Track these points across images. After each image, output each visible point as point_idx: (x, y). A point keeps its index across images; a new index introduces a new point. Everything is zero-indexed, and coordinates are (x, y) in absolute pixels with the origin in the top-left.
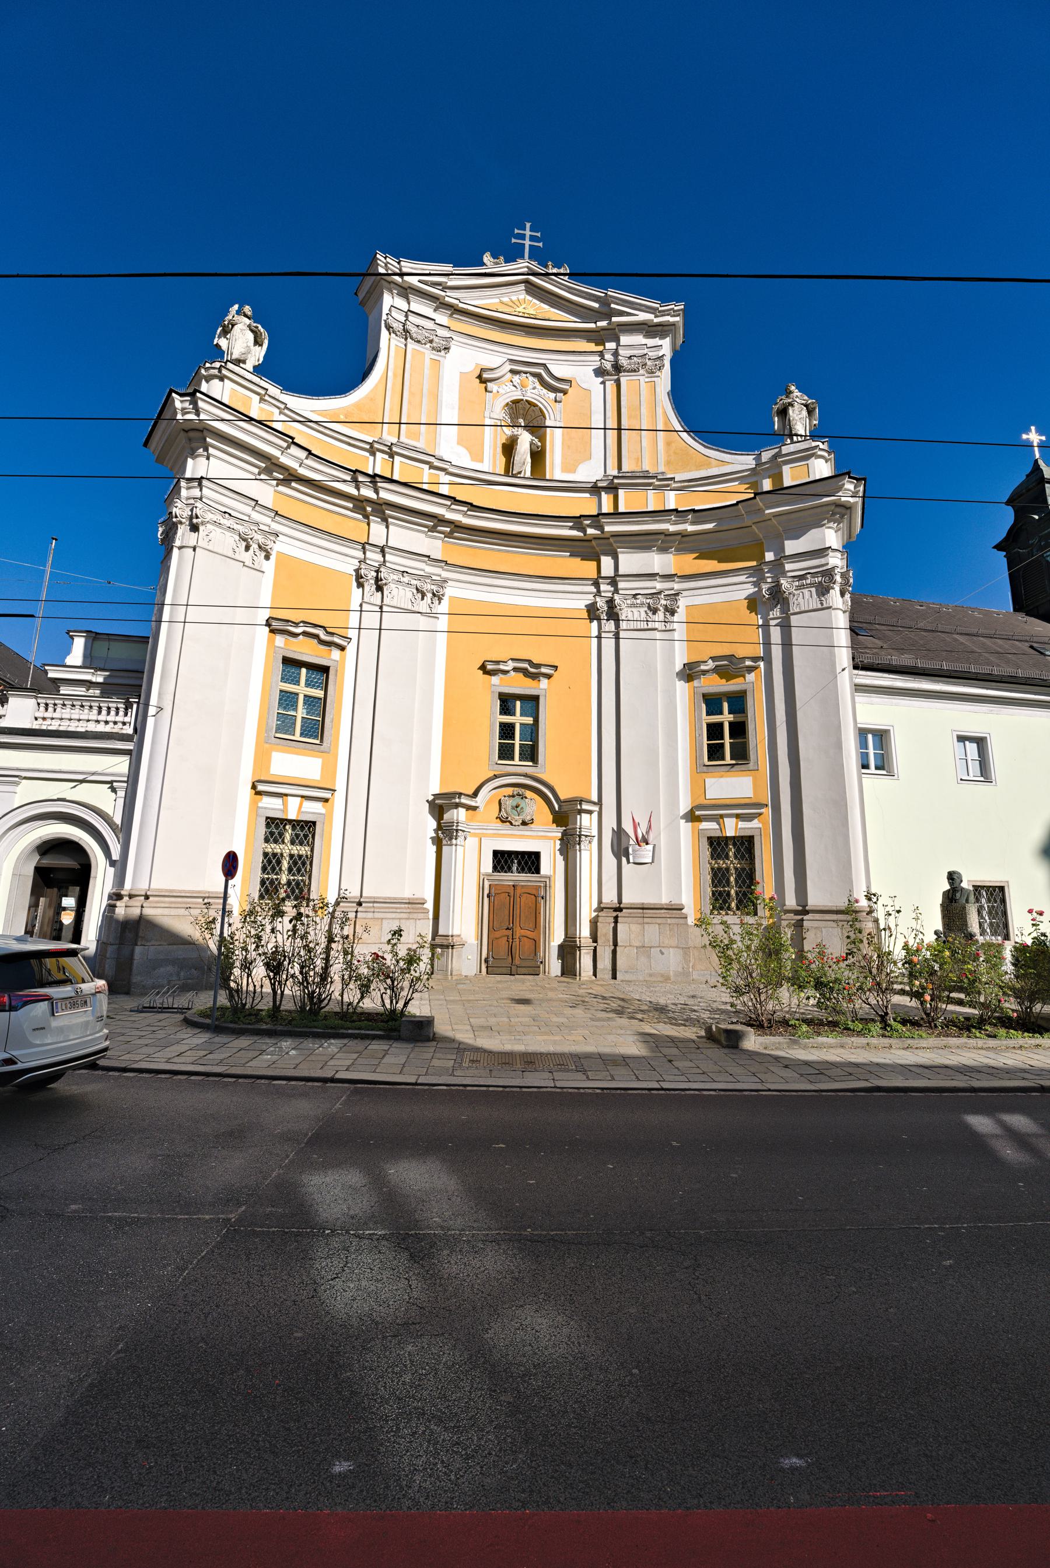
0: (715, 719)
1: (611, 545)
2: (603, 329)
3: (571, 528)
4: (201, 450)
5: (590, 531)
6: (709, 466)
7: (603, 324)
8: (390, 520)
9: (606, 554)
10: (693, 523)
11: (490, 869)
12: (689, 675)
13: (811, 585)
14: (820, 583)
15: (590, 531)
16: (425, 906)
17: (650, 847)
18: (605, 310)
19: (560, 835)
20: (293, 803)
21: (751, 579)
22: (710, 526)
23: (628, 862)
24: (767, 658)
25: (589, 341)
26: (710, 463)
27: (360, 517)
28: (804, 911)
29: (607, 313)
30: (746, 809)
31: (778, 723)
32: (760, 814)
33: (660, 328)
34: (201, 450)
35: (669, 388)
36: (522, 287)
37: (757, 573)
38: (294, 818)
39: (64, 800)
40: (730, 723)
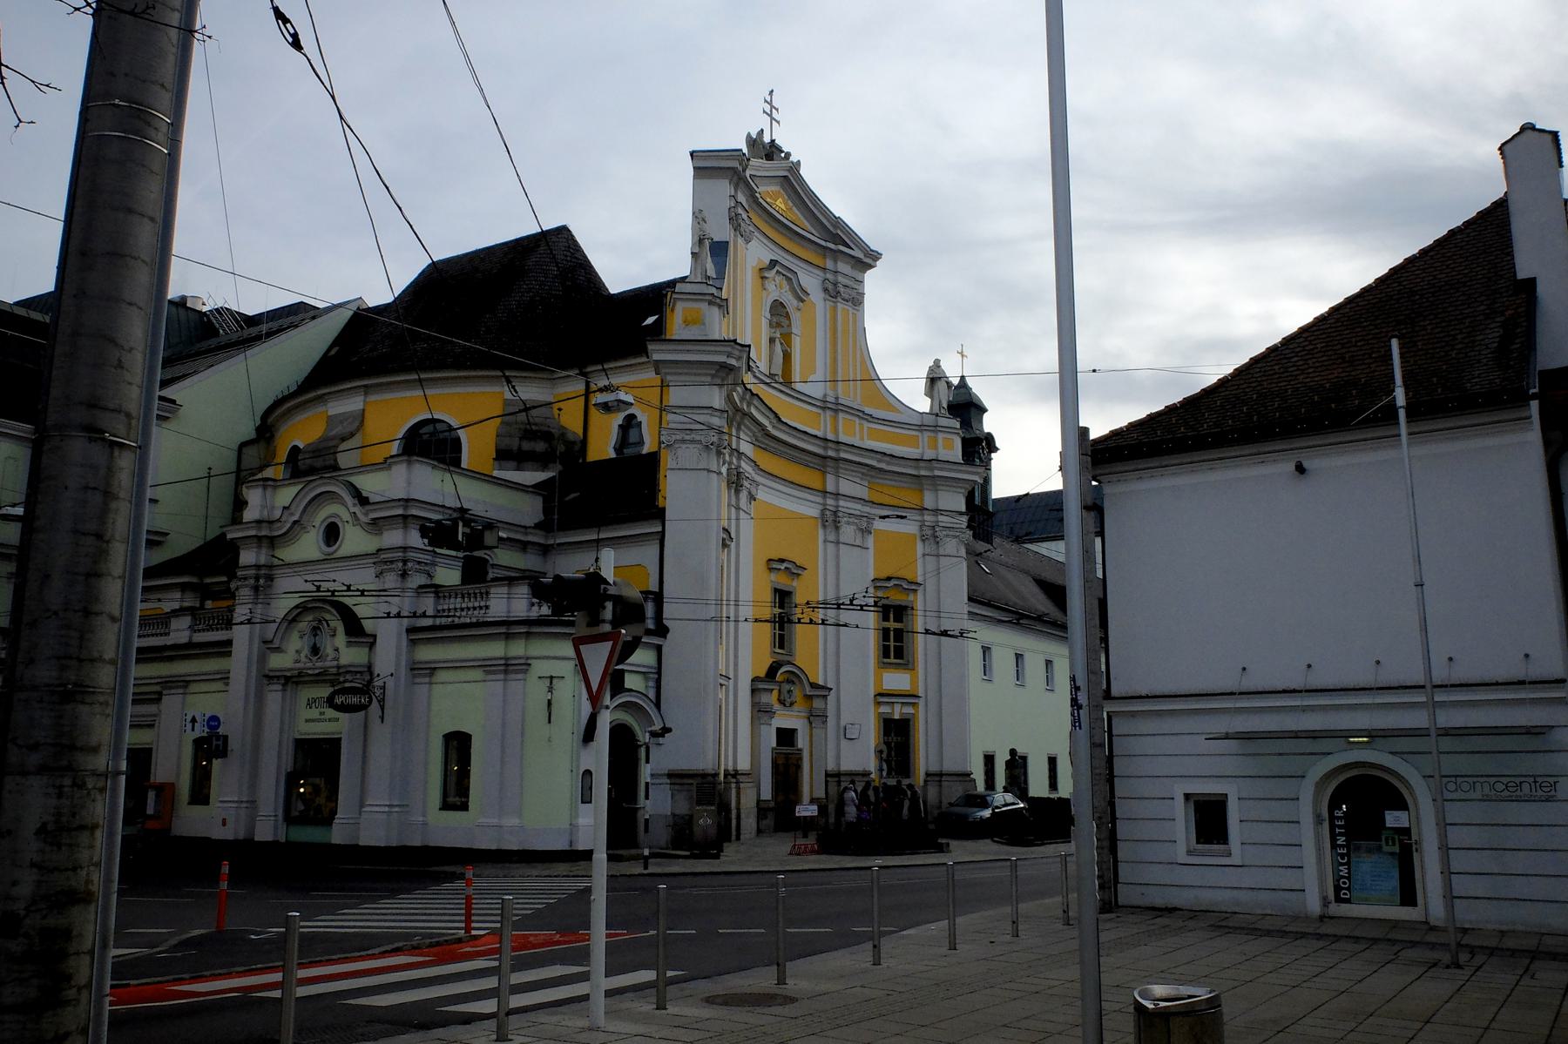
0: (886, 624)
20: (897, 708)
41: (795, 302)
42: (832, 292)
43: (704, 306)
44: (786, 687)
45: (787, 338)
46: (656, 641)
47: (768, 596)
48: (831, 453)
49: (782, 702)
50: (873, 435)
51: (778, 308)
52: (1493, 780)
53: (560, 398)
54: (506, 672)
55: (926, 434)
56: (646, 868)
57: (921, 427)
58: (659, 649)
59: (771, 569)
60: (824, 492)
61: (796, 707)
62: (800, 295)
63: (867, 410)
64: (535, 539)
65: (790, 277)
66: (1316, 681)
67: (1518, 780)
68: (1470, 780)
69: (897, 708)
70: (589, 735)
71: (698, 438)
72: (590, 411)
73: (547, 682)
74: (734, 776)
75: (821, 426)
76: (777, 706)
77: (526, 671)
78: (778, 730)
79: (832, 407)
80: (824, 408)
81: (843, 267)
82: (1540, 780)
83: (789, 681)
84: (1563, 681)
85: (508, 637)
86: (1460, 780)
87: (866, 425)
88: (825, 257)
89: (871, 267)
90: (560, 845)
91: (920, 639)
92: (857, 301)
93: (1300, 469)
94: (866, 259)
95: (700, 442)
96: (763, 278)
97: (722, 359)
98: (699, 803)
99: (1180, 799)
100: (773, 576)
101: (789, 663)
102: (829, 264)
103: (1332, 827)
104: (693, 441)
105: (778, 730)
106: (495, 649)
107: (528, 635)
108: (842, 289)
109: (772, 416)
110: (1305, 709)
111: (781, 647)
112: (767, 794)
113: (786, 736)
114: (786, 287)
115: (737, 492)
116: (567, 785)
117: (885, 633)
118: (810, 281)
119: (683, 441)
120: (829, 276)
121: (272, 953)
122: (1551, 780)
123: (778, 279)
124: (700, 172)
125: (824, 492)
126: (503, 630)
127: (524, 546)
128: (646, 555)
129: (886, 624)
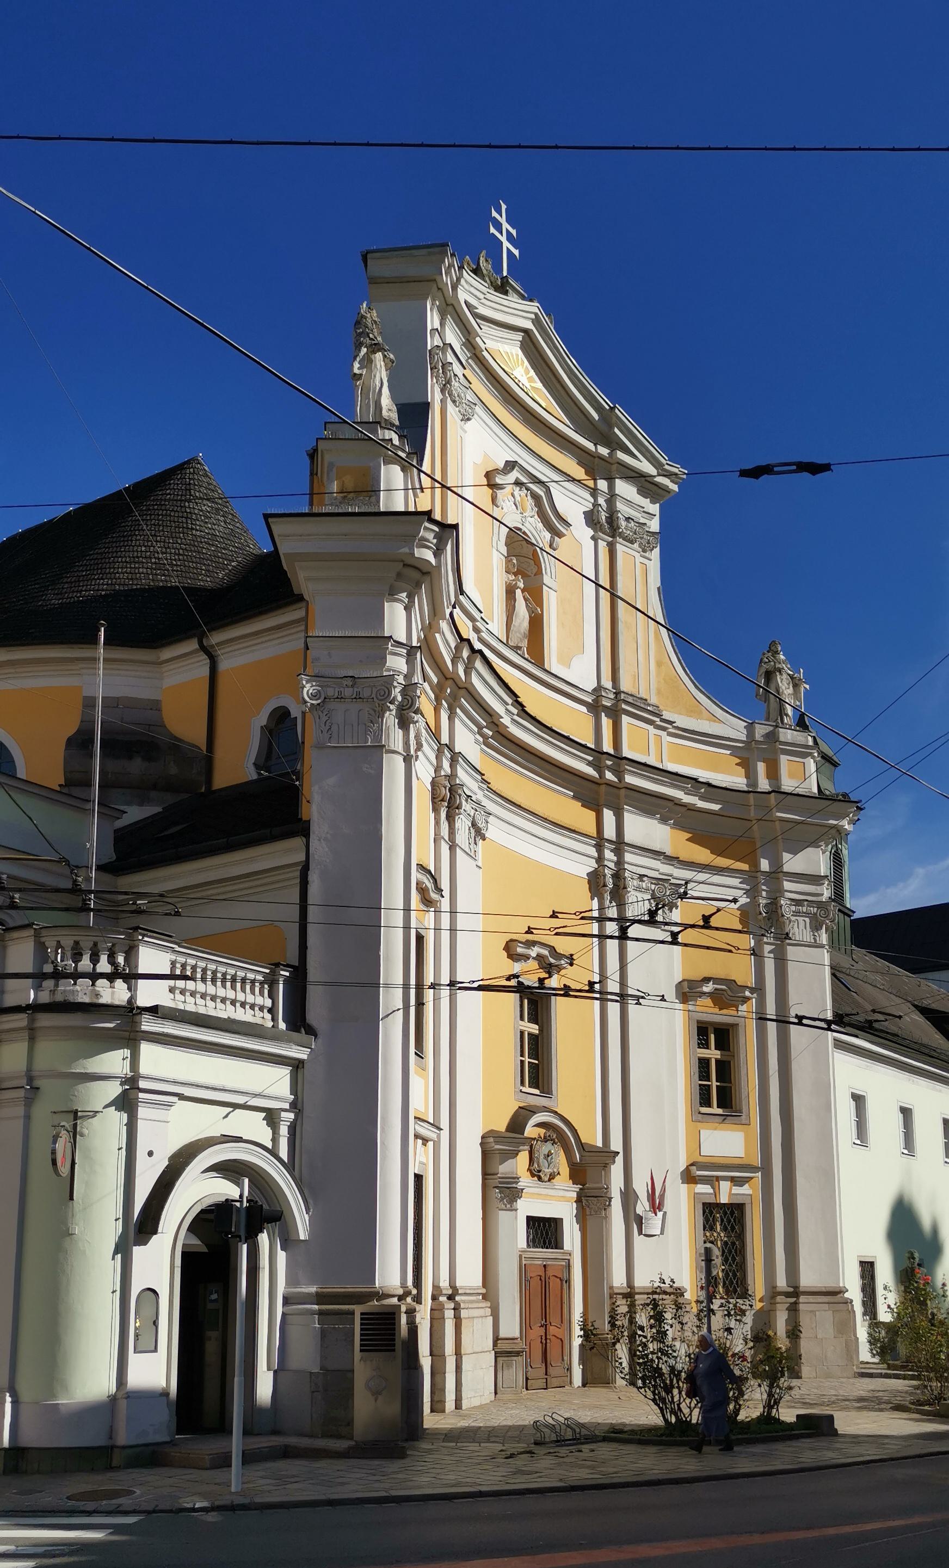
0: (704, 1053)
1: (618, 797)
2: (601, 458)
3: (590, 764)
4: (404, 595)
5: (609, 776)
6: (699, 715)
7: (604, 451)
8: (458, 711)
9: (609, 807)
10: (702, 798)
11: (525, 1245)
12: (684, 994)
13: (807, 914)
14: (815, 914)
15: (609, 776)
16: (846, 1295)
17: (662, 1213)
18: (603, 427)
19: (575, 1195)
20: (725, 1186)
21: (744, 886)
22: (716, 807)
23: (640, 1233)
24: (759, 989)
25: (580, 463)
26: (701, 712)
27: (433, 696)
28: (795, 1292)
29: (601, 433)
30: (736, 1171)
31: (771, 1072)
32: (752, 1178)
33: (656, 488)
34: (404, 595)
35: (659, 584)
36: (519, 336)
37: (752, 878)
38: (726, 1201)
39: (238, 1139)
40: (717, 1061)
45: (535, 595)
49: (535, 1174)
53: (171, 682)
62: (554, 523)
69: (725, 1186)
76: (525, 1181)
78: (531, 1221)
91: (825, 942)
98: (179, 1432)
101: (546, 1109)
105: (531, 1221)
111: (535, 1083)
112: (511, 1327)
113: (544, 1231)
115: (450, 818)
117: (703, 1032)
121: (413, 1330)
129: (704, 1053)
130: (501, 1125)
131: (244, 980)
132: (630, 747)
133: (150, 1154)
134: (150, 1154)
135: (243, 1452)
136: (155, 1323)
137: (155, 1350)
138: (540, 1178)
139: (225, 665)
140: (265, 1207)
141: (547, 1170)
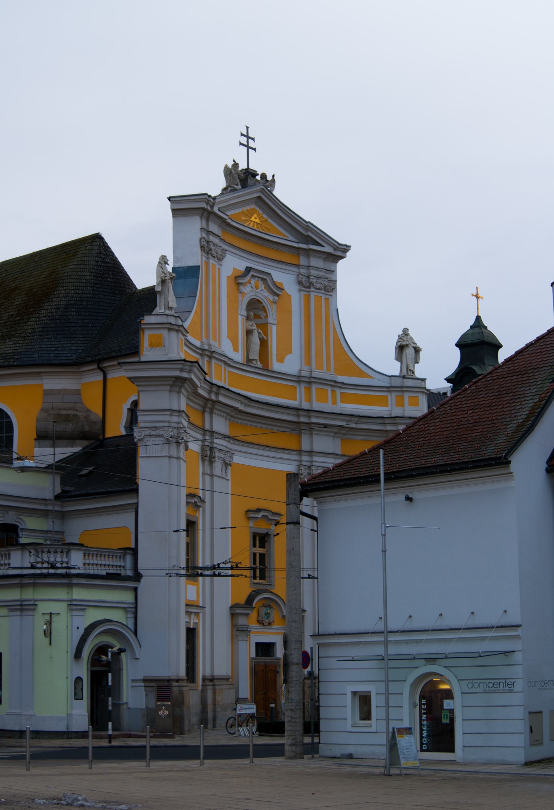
41: (271, 297)
42: (305, 285)
43: (165, 333)
44: (264, 610)
45: (264, 327)
46: (133, 584)
47: (247, 540)
48: (303, 419)
49: (260, 622)
50: (345, 399)
51: (255, 306)
52: (487, 681)
54: (21, 610)
55: (394, 395)
56: (110, 742)
57: (390, 389)
58: (136, 589)
59: (249, 518)
60: (300, 452)
61: (274, 626)
62: (276, 290)
63: (340, 378)
64: (56, 508)
65: (265, 278)
66: (479, 621)
67: (498, 681)
68: (478, 681)
70: (78, 655)
71: (161, 433)
72: (107, 396)
73: (48, 617)
74: (211, 680)
75: (298, 399)
77: (34, 610)
78: (258, 644)
79: (307, 381)
80: (299, 382)
81: (316, 262)
82: (507, 681)
83: (265, 606)
84: (518, 626)
85: (22, 586)
86: (474, 681)
87: (338, 391)
88: (299, 255)
89: (342, 258)
90: (61, 727)
92: (330, 288)
93: (409, 499)
94: (339, 252)
95: (162, 436)
96: (238, 284)
97: (177, 373)
99: (349, 696)
100: (251, 524)
102: (303, 261)
103: (421, 709)
104: (157, 436)
105: (258, 644)
106: (14, 595)
107: (34, 585)
108: (314, 280)
109: (242, 399)
110: (407, 642)
111: (262, 577)
113: (265, 649)
114: (262, 286)
115: (211, 462)
116: (65, 687)
118: (285, 278)
119: (150, 436)
120: (303, 271)
122: (512, 681)
123: (253, 282)
124: (176, 212)
125: (300, 452)
126: (17, 581)
127: (45, 514)
128: (125, 520)
130: (242, 600)
131: (116, 556)
132: (317, 400)
133: (78, 628)
134: (78, 628)
135: (135, 491)
136: (82, 689)
137: (82, 699)
138: (263, 624)
139: (109, 376)
140: (148, 319)
141: (267, 620)
